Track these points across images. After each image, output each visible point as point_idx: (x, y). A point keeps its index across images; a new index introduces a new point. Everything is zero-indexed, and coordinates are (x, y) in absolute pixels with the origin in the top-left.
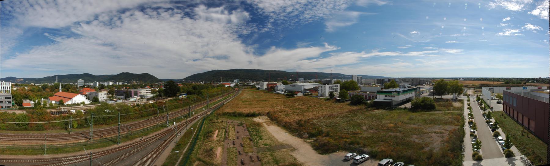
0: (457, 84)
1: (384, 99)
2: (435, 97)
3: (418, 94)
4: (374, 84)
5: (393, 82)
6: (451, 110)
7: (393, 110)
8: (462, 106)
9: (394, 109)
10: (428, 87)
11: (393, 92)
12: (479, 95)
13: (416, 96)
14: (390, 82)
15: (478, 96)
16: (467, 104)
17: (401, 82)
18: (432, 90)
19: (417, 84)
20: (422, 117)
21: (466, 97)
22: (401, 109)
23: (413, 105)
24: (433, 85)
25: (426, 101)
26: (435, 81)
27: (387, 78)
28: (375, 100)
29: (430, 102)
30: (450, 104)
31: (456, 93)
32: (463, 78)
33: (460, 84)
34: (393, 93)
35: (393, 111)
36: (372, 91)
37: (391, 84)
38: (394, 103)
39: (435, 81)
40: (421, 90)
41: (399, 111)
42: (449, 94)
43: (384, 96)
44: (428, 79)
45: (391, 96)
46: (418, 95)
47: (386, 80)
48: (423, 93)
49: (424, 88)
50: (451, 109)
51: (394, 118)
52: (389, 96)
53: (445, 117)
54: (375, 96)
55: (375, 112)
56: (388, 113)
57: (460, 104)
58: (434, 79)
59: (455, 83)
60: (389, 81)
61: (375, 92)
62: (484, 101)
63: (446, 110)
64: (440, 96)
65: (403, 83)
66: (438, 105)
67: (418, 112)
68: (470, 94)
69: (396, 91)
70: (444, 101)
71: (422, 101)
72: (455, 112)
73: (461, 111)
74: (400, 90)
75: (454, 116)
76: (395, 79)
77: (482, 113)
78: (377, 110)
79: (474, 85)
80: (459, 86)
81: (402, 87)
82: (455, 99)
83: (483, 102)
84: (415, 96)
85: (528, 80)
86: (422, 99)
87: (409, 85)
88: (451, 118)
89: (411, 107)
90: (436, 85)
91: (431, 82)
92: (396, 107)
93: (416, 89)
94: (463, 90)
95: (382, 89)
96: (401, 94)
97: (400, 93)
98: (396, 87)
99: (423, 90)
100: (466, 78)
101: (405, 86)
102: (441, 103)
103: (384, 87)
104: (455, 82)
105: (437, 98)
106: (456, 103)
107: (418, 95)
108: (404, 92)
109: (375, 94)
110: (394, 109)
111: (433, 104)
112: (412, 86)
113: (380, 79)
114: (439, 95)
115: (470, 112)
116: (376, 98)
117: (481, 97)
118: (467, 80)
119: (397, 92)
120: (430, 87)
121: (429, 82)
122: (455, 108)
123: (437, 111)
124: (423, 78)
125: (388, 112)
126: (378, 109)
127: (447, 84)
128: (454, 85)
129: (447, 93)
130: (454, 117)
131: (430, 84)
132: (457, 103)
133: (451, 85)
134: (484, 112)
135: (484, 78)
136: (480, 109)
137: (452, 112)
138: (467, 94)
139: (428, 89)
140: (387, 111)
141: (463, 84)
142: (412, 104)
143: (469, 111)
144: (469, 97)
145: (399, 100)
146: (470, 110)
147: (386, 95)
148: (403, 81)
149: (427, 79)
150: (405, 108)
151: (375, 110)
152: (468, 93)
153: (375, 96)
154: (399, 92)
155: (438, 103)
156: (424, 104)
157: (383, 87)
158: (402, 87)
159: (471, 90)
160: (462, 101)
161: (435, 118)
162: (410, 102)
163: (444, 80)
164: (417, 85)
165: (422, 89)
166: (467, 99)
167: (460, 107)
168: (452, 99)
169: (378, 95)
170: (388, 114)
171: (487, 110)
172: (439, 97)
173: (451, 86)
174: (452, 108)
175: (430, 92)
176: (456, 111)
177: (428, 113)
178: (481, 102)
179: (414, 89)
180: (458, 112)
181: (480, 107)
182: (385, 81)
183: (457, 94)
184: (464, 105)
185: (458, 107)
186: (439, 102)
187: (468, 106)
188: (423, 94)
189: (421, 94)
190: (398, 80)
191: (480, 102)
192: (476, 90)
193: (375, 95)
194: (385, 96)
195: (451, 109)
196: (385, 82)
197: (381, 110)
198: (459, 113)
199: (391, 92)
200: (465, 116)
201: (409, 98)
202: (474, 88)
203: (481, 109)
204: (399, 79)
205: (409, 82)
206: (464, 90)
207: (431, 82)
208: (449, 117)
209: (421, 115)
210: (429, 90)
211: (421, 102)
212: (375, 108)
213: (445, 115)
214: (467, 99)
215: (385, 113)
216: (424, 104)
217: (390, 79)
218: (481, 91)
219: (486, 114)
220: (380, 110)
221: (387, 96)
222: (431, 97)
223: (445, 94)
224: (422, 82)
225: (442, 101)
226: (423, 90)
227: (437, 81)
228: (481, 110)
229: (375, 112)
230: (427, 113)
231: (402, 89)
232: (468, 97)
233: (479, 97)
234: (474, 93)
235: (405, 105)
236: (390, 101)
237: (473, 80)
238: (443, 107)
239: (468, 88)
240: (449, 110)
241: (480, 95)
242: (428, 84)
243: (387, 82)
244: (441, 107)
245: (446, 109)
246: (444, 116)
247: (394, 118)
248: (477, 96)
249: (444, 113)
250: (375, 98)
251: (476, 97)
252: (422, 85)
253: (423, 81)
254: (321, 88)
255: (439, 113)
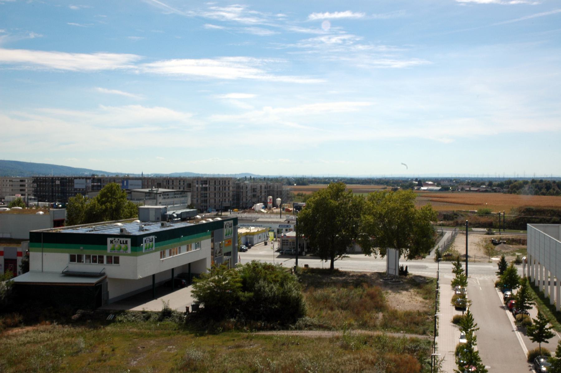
0: (406, 209)
1: (67, 274)
2: (302, 262)
3: (230, 249)
4: (18, 203)
5: (112, 191)
6: (375, 327)
7: (108, 323)
8: (422, 310)
9: (113, 321)
10: (276, 219)
11: (109, 240)
12: (510, 259)
13: (221, 260)
14: (98, 194)
15: (509, 265)
16: (454, 300)
17: (151, 196)
18: (293, 234)
19: (227, 204)
20: (242, 354)
21: (450, 266)
22: (147, 316)
23: (201, 299)
24: (298, 208)
25: (261, 282)
26: (306, 191)
27: (87, 174)
28: (22, 278)
29: (282, 285)
30: (372, 297)
31: (400, 247)
32: (437, 181)
33: (418, 207)
34: (109, 246)
35: (109, 328)
36: (8, 236)
37: (103, 203)
38: (113, 293)
39: (308, 193)
40: (242, 231)
41: (272, 61)
42: (367, 252)
43: (66, 256)
44: (276, 184)
45: (101, 257)
46: (228, 254)
47: (78, 185)
48: (249, 244)
49: (255, 223)
50: (378, 323)
51: (112, 362)
52: (88, 257)
53: (345, 358)
54: (20, 260)
55: (13, 341)
56: (81, 342)
57: (420, 299)
58: (304, 184)
59: (395, 201)
60: (94, 189)
61: (18, 241)
62: (536, 289)
63: (350, 326)
64: (329, 261)
65: (160, 199)
66: (317, 301)
67: (226, 330)
68: (466, 256)
69: (123, 235)
70: (345, 284)
71: (244, 281)
72: (396, 335)
73: (424, 333)
74: (141, 229)
75: (390, 356)
76: (125, 180)
77: (526, 351)
78: (29, 328)
79: (487, 213)
80: (417, 216)
81: (152, 216)
82: (394, 277)
83: (533, 294)
84: (213, 260)
85: (525, 182)
86: (244, 271)
87: (189, 207)
88: (373, 363)
89: (195, 307)
90: (310, 211)
91: (287, 198)
92: (120, 308)
93: (218, 225)
94: (434, 233)
95: (58, 223)
96: (149, 250)
97: (144, 245)
98: (126, 217)
99: (253, 229)
100: (450, 180)
101: (169, 213)
102: (332, 292)
103: (69, 215)
104: (395, 196)
105: (313, 271)
106: (398, 295)
107: (228, 254)
108: (161, 237)
109: (21, 248)
110: (110, 317)
111: (294, 294)
112: (201, 211)
113: (53, 180)
114: (323, 257)
115: (464, 341)
116: (26, 268)
117: (520, 271)
118: (453, 191)
119: (129, 240)
120: (283, 219)
121: (280, 194)
122: (394, 315)
123: (310, 327)
124: (253, 180)
125: (81, 334)
126: (30, 321)
127: (358, 208)
128: (393, 210)
129: (358, 247)
130: (390, 360)
131: (286, 206)
132: (404, 292)
133: (378, 209)
134: (536, 345)
135: (541, 181)
136: (515, 327)
137: (379, 337)
138: (455, 255)
139: (276, 227)
140: (79, 329)
141: (437, 208)
142: (195, 294)
143: (462, 337)
144: (463, 266)
145: (140, 277)
146: (466, 330)
147: (76, 252)
148: (161, 190)
149: (270, 183)
150: (167, 313)
151: (16, 325)
152: (459, 247)
153: (20, 260)
154: (136, 241)
155: (319, 292)
156: (252, 294)
157: (63, 214)
158: (152, 216)
159: (471, 238)
160: (428, 286)
161: (299, 362)
162: (190, 288)
163: (348, 186)
164: (226, 209)
165: (247, 227)
166: (453, 277)
167: (419, 313)
168: (380, 275)
169: (31, 254)
170: (83, 345)
171: (551, 336)
172: (325, 264)
173: (381, 217)
174: (380, 315)
175: (284, 242)
176: (398, 331)
177: (270, 338)
178: (523, 293)
179: (209, 224)
180: (408, 336)
181: (518, 321)
182: (76, 186)
183: (406, 252)
184: (437, 303)
185: (408, 314)
186: (318, 285)
187: (458, 309)
188: (250, 252)
189: (244, 251)
190: (140, 182)
191: (515, 292)
192: (496, 236)
193: (20, 254)
194: (72, 259)
195: (378, 323)
196: (76, 192)
197: (50, 327)
198: (413, 341)
199: (101, 240)
200: (440, 358)
201: (183, 266)
202: (489, 226)
203: (519, 329)
204: (146, 181)
205: (189, 194)
206: (442, 235)
207: (287, 198)
208: (366, 361)
209: (238, 347)
210: (279, 231)
211: (239, 285)
212: (18, 318)
213: (345, 347)
214: (453, 277)
215: (67, 340)
216: (252, 294)
217: (99, 180)
218: (523, 242)
219: (546, 355)
220: (41, 327)
221: (80, 260)
222: (289, 263)
223: (348, 249)
224: (249, 194)
225: (335, 283)
226: (253, 229)
227: (313, 190)
228: (519, 334)
229: (13, 341)
230: (266, 338)
231: (156, 228)
232: (458, 266)
233: (513, 272)
234: (486, 248)
235: (166, 298)
236: (94, 281)
237: (486, 191)
238: (337, 311)
239: (457, 224)
240: (364, 325)
241: (518, 262)
242: (274, 205)
243: (84, 192)
244: (332, 309)
245: (353, 322)
246: (341, 350)
247: (112, 362)
248: (502, 265)
249: (344, 336)
250: (19, 269)
251: (497, 268)
252: (247, 207)
253: (254, 190)
254: (78, 180)
255: (320, 339)
